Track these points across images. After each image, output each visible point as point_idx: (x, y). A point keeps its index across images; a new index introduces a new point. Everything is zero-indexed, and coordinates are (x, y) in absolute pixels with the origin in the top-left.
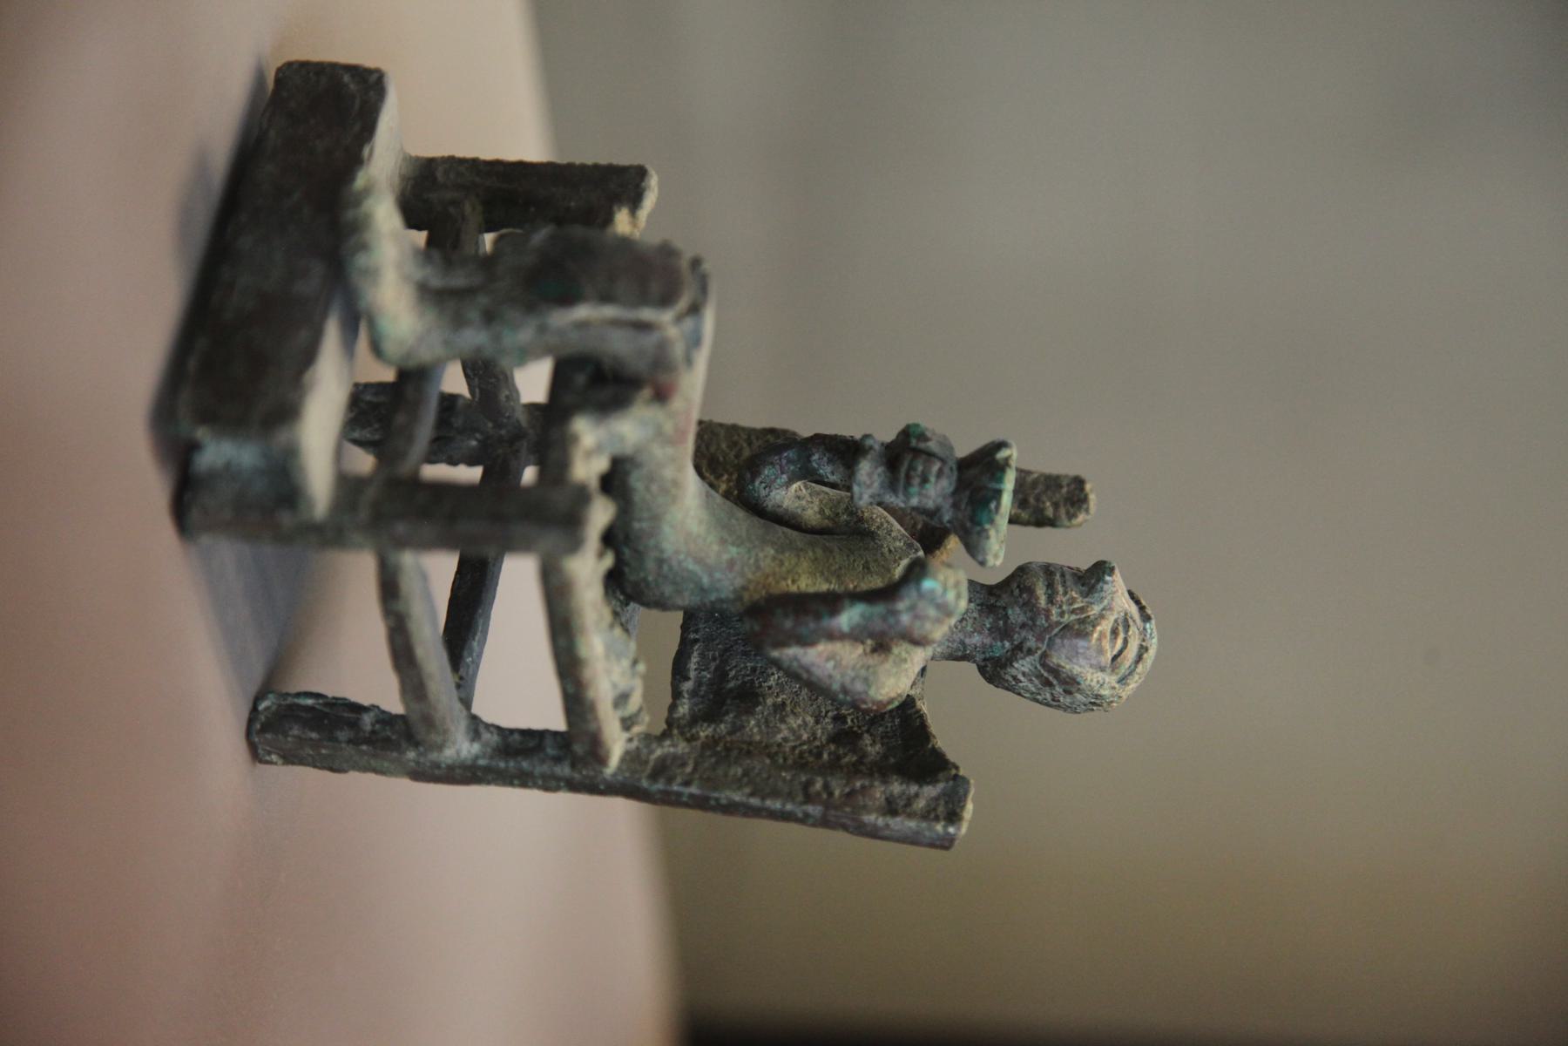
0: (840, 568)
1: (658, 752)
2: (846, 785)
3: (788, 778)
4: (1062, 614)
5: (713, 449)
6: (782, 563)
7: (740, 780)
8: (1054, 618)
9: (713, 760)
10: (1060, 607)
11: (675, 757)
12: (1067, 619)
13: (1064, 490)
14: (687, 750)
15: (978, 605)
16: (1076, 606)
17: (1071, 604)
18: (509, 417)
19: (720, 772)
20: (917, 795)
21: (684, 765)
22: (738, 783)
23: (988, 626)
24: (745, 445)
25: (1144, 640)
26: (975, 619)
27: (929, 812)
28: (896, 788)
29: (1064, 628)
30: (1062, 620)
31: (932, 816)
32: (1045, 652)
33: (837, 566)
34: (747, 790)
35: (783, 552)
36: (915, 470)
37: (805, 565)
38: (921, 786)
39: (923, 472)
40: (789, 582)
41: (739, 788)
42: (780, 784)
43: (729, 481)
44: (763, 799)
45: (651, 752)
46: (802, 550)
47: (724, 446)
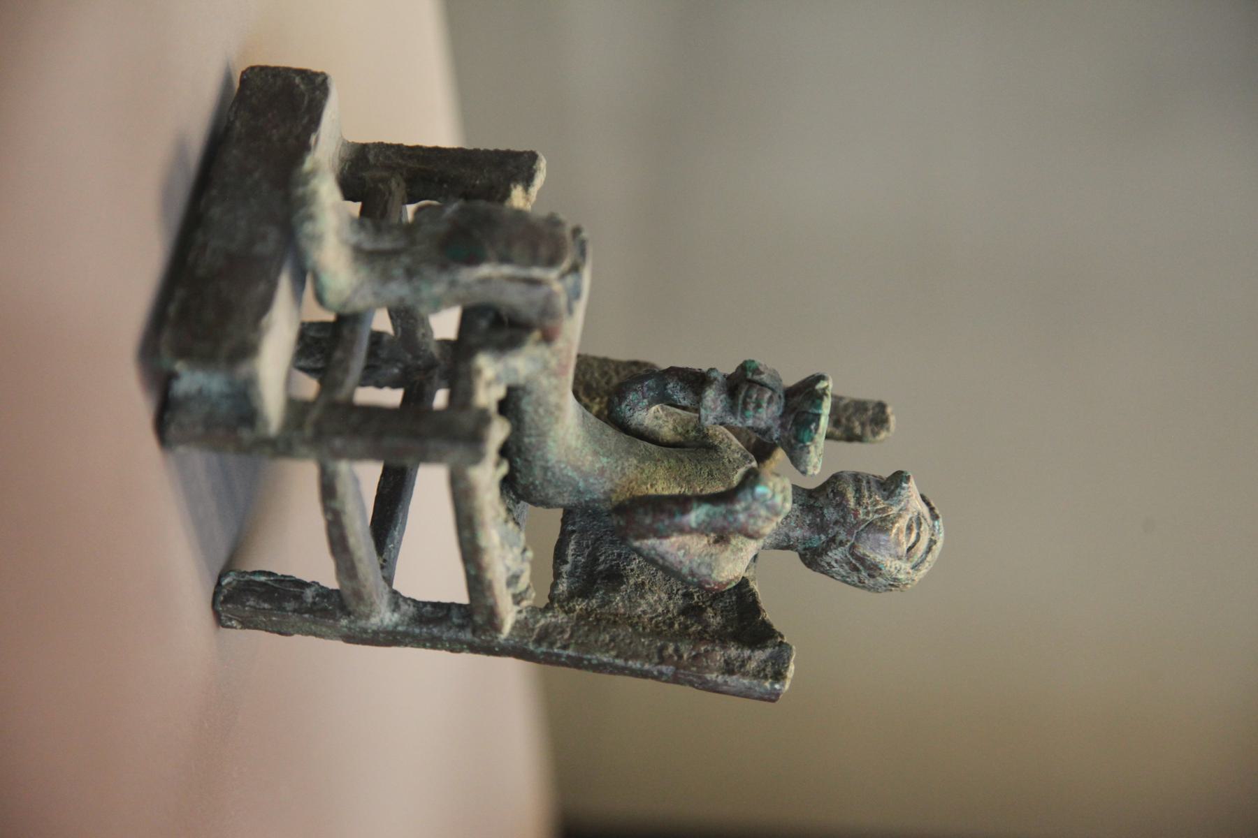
0: (690, 475)
1: (542, 622)
2: (693, 649)
3: (646, 643)
4: (867, 513)
5: (588, 377)
6: (643, 470)
7: (607, 645)
8: (861, 517)
9: (586, 628)
10: (866, 508)
12: (871, 517)
14: (565, 620)
15: (800, 505)
16: (879, 507)
17: (875, 506)
19: (592, 638)
22: (606, 648)
23: (808, 522)
25: (933, 535)
26: (798, 516)
27: (759, 672)
28: (733, 652)
29: (869, 524)
30: (867, 518)
31: (762, 675)
32: (854, 543)
33: (687, 474)
34: (613, 653)
35: (644, 463)
36: (751, 397)
37: (661, 472)
38: (753, 651)
39: (757, 399)
40: (649, 486)
41: (607, 651)
42: (640, 648)
43: (600, 403)
44: (626, 660)
45: (537, 622)
46: (659, 460)
47: (596, 375)
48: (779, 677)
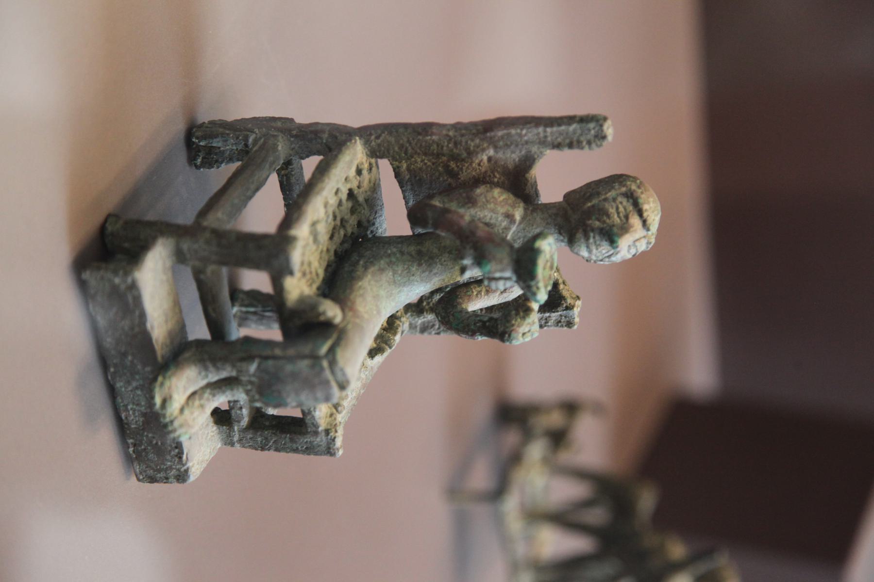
1: (420, 321)
11: (429, 322)
13: (593, 132)
18: (222, 436)
20: (549, 317)
21: (433, 325)
24: (408, 145)
46: (452, 268)
47: (396, 149)
48: (571, 325)
